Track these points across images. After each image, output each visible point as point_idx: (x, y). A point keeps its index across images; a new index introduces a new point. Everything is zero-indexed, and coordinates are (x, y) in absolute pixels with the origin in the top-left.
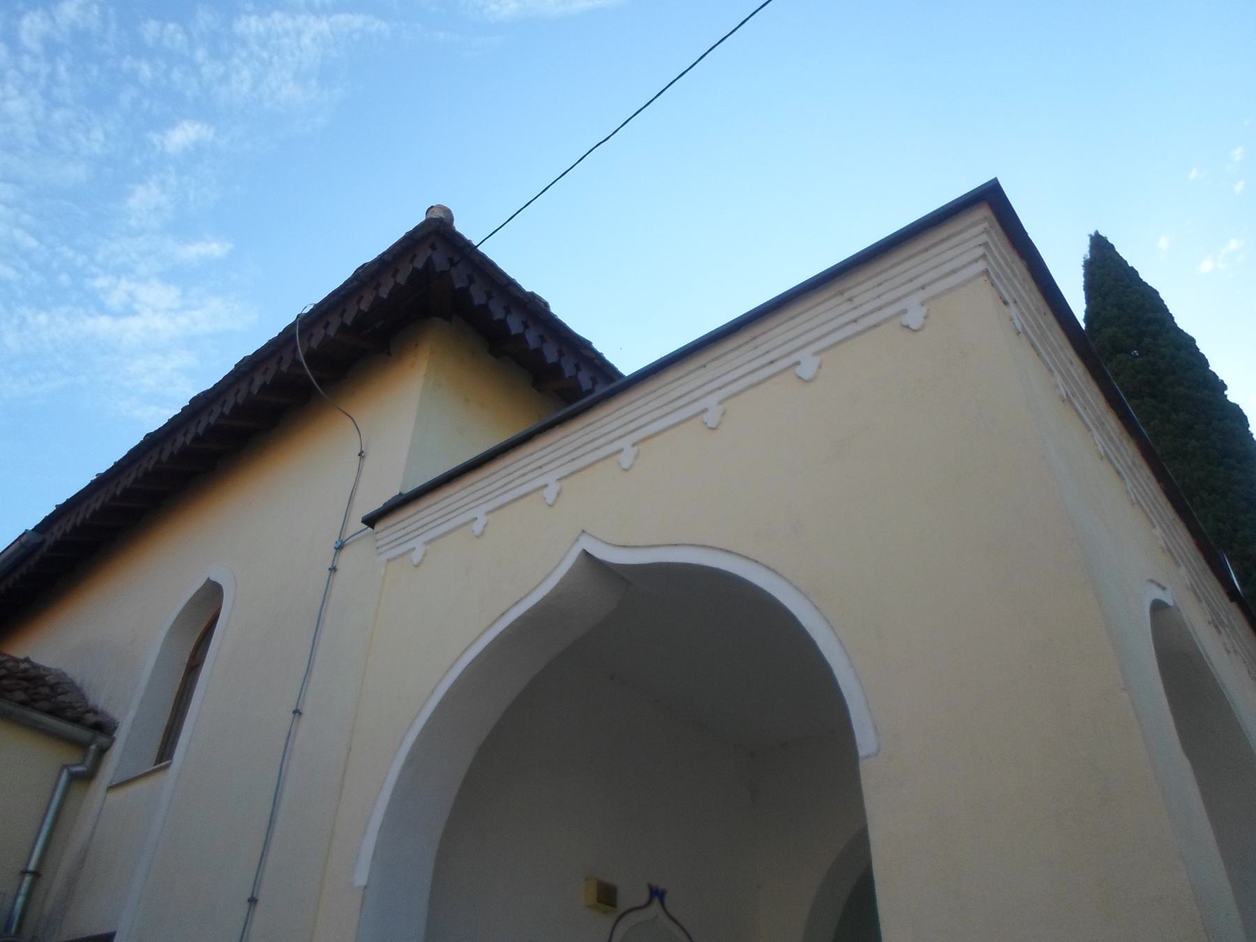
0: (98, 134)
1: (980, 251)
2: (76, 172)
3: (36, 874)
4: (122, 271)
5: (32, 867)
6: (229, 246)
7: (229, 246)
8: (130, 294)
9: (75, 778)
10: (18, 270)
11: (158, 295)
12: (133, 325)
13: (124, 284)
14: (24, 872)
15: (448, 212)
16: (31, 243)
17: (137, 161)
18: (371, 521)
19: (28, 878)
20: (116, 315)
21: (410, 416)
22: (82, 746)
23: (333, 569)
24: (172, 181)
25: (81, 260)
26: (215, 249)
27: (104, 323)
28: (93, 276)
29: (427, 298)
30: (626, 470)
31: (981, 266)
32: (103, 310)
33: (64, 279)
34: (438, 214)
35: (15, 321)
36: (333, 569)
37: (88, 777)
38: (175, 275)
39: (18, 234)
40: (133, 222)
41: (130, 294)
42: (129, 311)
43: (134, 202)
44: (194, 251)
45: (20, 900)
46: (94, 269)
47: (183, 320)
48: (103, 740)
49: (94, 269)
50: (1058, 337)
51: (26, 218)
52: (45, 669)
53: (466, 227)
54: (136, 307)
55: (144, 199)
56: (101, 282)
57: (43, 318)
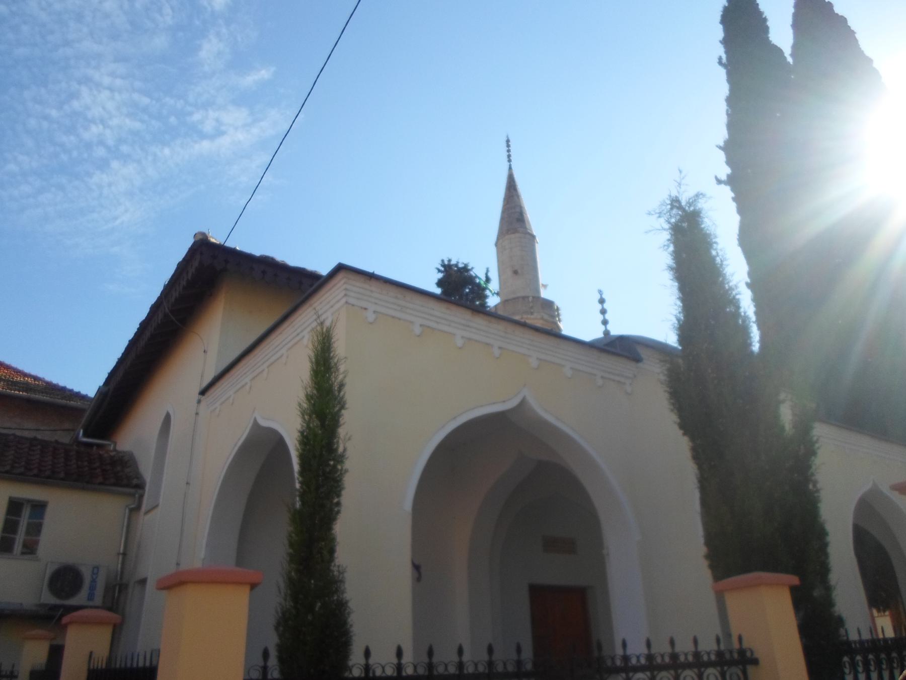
0: (167, 10)
1: (344, 292)
2: (160, 42)
3: (124, 554)
4: (207, 105)
5: (121, 551)
6: (273, 69)
7: (273, 69)
8: (217, 120)
9: (131, 510)
10: (142, 121)
11: (235, 116)
12: (224, 142)
13: (212, 114)
14: (119, 554)
15: (203, 234)
16: (145, 100)
17: (197, 23)
18: (203, 392)
19: (121, 557)
20: (212, 137)
21: (217, 334)
22: (133, 495)
23: (197, 414)
24: (224, 30)
25: (180, 104)
26: (265, 74)
27: (206, 145)
28: (191, 114)
29: (208, 275)
30: (371, 323)
31: (344, 300)
32: (203, 136)
33: (173, 120)
34: (199, 237)
35: (150, 158)
36: (197, 414)
37: (138, 508)
38: (243, 99)
39: (136, 96)
40: (206, 68)
41: (217, 120)
42: (219, 132)
43: (203, 54)
44: (250, 80)
45: (120, 566)
46: (189, 109)
47: (255, 131)
48: (140, 491)
49: (189, 109)
50: (433, 304)
51: (138, 84)
52: (124, 452)
53: (216, 238)
54: (223, 128)
55: (210, 50)
56: (197, 117)
57: (167, 151)
